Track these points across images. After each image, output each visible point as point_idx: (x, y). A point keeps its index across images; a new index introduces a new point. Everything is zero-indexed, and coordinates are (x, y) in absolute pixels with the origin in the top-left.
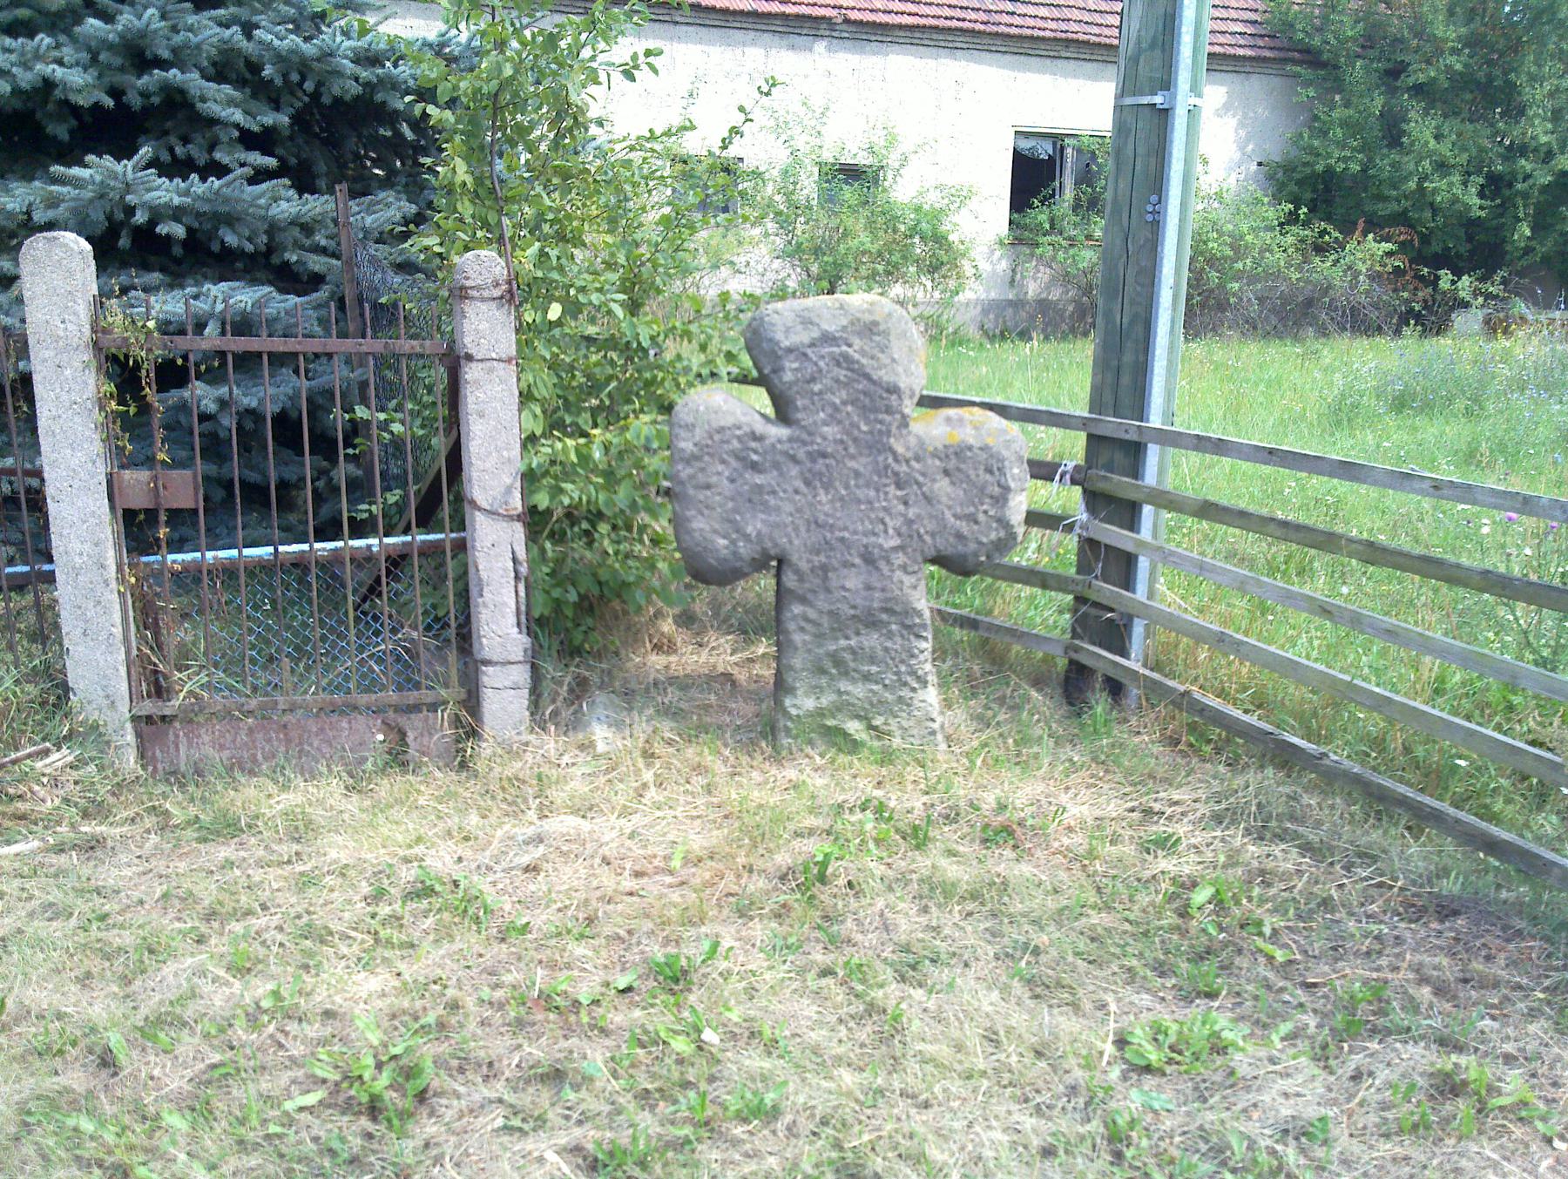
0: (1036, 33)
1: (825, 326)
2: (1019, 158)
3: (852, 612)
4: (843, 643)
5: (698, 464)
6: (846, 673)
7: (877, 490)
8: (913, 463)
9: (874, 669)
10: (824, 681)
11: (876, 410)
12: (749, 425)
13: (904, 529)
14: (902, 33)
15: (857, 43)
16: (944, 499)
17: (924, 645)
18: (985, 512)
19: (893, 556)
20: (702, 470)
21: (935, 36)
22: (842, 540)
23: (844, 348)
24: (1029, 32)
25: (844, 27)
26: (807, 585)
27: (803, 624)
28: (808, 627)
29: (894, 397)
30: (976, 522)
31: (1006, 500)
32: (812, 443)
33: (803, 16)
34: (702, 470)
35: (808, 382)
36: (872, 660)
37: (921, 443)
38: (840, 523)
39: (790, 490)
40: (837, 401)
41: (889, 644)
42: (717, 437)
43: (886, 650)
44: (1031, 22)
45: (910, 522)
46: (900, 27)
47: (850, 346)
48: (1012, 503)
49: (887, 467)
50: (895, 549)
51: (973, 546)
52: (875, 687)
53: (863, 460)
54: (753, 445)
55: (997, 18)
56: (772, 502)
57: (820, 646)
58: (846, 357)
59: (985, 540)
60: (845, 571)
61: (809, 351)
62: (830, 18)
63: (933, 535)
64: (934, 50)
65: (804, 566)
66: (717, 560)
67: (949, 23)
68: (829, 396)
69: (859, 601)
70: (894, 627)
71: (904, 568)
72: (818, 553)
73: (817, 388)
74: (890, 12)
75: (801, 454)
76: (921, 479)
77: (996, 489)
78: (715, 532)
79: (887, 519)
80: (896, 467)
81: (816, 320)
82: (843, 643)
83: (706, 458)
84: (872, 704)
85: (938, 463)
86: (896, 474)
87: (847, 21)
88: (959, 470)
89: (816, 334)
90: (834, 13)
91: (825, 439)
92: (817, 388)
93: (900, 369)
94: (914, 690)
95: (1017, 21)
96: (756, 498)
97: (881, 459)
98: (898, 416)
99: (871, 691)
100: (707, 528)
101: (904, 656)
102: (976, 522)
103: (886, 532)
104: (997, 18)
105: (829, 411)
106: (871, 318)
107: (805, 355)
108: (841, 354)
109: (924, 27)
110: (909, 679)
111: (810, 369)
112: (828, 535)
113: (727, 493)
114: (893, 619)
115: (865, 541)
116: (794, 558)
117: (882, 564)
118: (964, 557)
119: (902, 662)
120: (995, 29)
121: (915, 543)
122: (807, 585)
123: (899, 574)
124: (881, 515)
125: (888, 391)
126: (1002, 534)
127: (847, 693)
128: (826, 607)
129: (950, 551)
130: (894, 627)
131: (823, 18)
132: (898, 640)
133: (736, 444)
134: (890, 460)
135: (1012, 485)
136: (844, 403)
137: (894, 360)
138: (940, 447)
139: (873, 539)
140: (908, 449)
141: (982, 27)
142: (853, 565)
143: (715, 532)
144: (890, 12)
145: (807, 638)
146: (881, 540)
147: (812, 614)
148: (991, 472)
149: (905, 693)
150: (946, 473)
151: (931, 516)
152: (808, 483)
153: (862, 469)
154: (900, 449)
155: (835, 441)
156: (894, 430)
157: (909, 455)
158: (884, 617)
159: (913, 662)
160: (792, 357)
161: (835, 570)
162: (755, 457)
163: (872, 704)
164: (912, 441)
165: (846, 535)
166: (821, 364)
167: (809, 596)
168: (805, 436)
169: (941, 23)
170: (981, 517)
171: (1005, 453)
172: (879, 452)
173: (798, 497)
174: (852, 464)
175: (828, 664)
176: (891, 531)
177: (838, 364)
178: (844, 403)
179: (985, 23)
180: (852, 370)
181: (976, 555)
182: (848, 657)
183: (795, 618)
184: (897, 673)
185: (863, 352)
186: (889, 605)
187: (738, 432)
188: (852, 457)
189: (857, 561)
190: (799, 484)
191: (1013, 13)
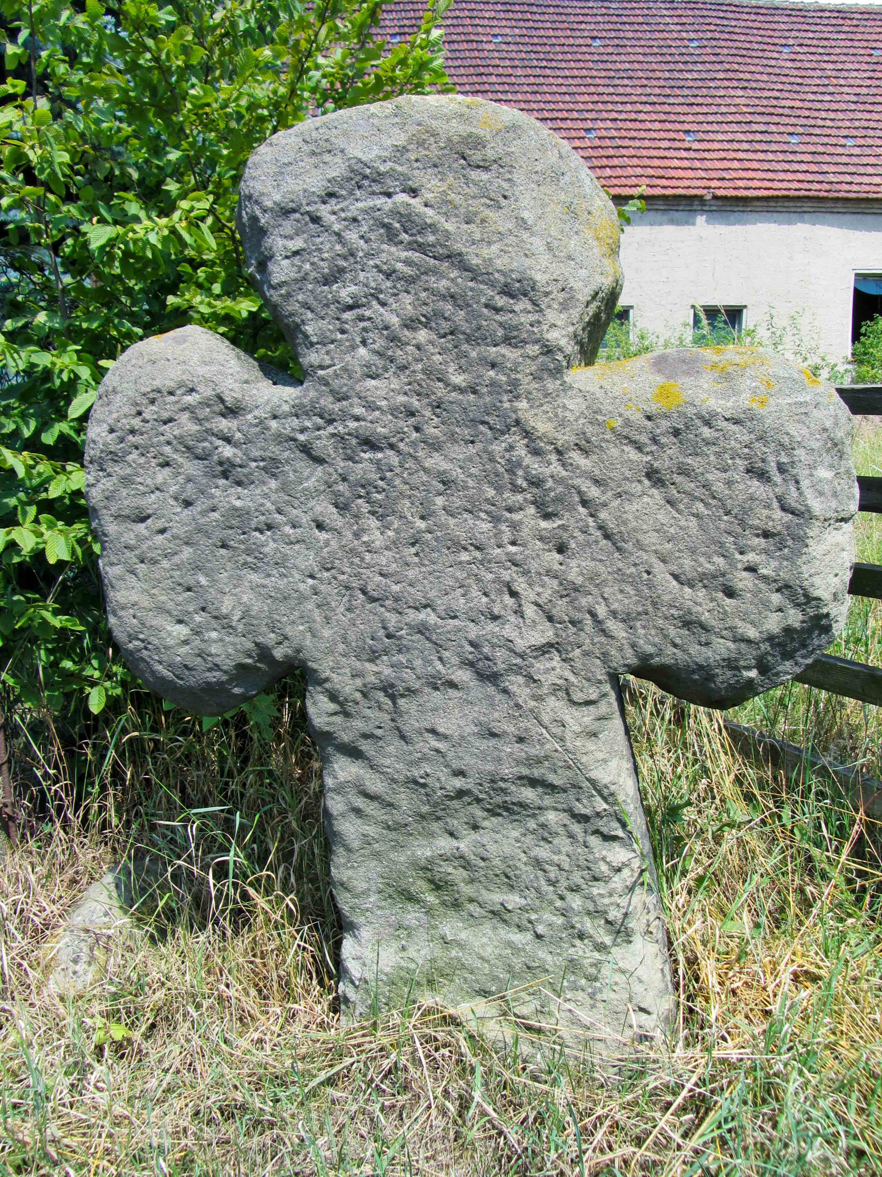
0: (871, 196)
1: (356, 151)
2: (858, 295)
3: (458, 783)
4: (445, 844)
5: (117, 469)
6: (456, 905)
7: (496, 520)
8: (576, 457)
9: (514, 900)
10: (413, 916)
11: (476, 338)
12: (208, 381)
13: (561, 608)
14: (758, 204)
15: (725, 214)
16: (651, 539)
17: (618, 854)
18: (751, 569)
19: (539, 666)
20: (126, 481)
21: (786, 204)
22: (422, 629)
23: (402, 198)
24: (864, 195)
25: (713, 202)
26: (358, 724)
27: (360, 802)
28: (370, 808)
29: (523, 304)
30: (730, 593)
31: (801, 540)
32: (345, 415)
33: (680, 196)
34: (126, 481)
35: (327, 281)
36: (510, 881)
37: (594, 414)
38: (416, 594)
39: (305, 519)
40: (394, 320)
41: (543, 852)
42: (149, 412)
43: (538, 863)
44: (867, 188)
45: (570, 591)
46: (758, 199)
47: (414, 192)
48: (815, 549)
49: (513, 467)
50: (544, 650)
51: (723, 647)
52: (518, 938)
53: (460, 452)
54: (224, 424)
55: (838, 187)
56: (269, 544)
57: (399, 846)
58: (408, 220)
59: (752, 633)
60: (437, 697)
61: (324, 211)
62: (702, 196)
63: (627, 620)
64: (786, 215)
65: (348, 687)
66: (170, 666)
67: (797, 193)
68: (374, 310)
69: (468, 761)
70: (551, 817)
71: (565, 691)
72: (374, 656)
73: (346, 292)
74: (749, 189)
75: (323, 444)
76: (594, 492)
77: (778, 514)
78: (162, 610)
79: (520, 585)
80: (535, 466)
81: (340, 143)
82: (445, 844)
83: (134, 456)
84: (510, 969)
85: (633, 454)
86: (536, 482)
87: (715, 197)
88: (684, 471)
89: (337, 168)
90: (705, 192)
91: (371, 407)
92: (346, 292)
93: (537, 244)
94: (600, 947)
95: (855, 188)
96: (235, 538)
97: (497, 448)
98: (533, 349)
99: (510, 944)
100: (145, 602)
101: (577, 878)
102: (730, 593)
103: (519, 612)
104: (838, 187)
105: (379, 343)
106: (464, 129)
107: (316, 220)
108: (395, 213)
109: (778, 197)
110: (588, 925)
111: (329, 247)
112: (392, 619)
113: (178, 530)
114: (548, 801)
115: (473, 631)
116: (323, 667)
117: (516, 683)
118: (704, 670)
119: (575, 889)
120: (836, 195)
121: (588, 635)
122: (358, 724)
123: (554, 706)
124: (506, 575)
125: (507, 291)
126: (795, 618)
127: (461, 946)
128: (401, 770)
129: (670, 656)
130: (551, 817)
131: (696, 196)
132: (562, 842)
133: (187, 425)
134: (521, 451)
135: (816, 505)
136: (410, 324)
137: (522, 224)
138: (637, 417)
139: (492, 627)
140: (562, 424)
141: (826, 194)
142: (452, 685)
143: (162, 610)
144: (749, 189)
145: (371, 830)
146: (508, 631)
147: (376, 784)
148: (762, 476)
149: (583, 951)
150: (653, 475)
151: (621, 577)
152: (342, 507)
153: (457, 473)
154: (542, 426)
155: (394, 411)
156: (526, 383)
157: (564, 438)
158: (529, 794)
159: (597, 890)
160: (288, 226)
161: (411, 692)
162: (228, 451)
163: (510, 969)
164: (574, 405)
165: (430, 617)
166: (352, 236)
167: (365, 746)
168: (327, 402)
169: (792, 193)
170: (743, 581)
171: (796, 430)
172: (499, 433)
173: (323, 536)
174: (435, 462)
175: (420, 886)
176: (530, 611)
177: (391, 236)
178: (410, 324)
179: (826, 191)
180: (421, 248)
181: (732, 664)
182: (458, 874)
183: (339, 789)
184: (564, 913)
185: (445, 206)
186: (536, 773)
187: (189, 399)
188: (435, 446)
189: (463, 676)
190: (324, 508)
191: (851, 183)
